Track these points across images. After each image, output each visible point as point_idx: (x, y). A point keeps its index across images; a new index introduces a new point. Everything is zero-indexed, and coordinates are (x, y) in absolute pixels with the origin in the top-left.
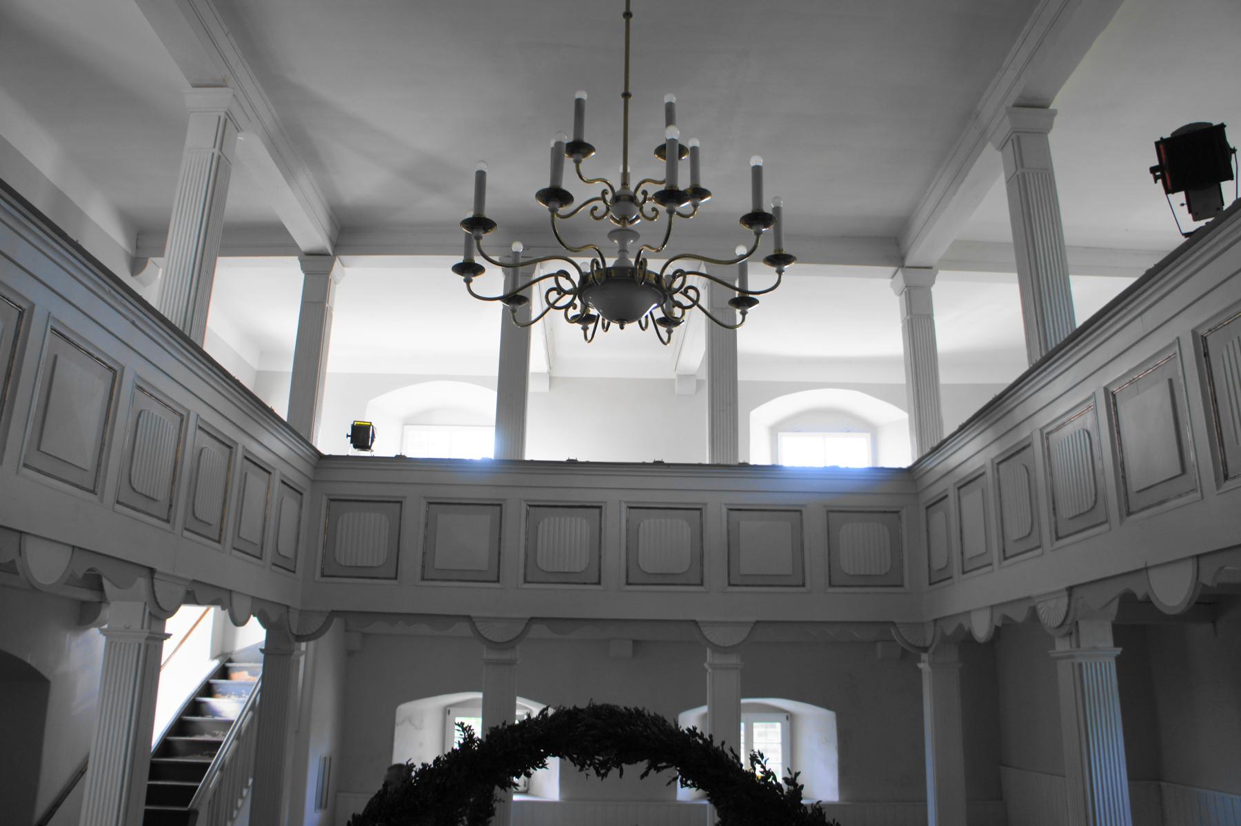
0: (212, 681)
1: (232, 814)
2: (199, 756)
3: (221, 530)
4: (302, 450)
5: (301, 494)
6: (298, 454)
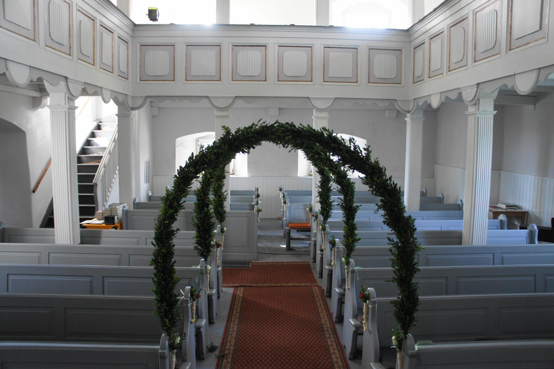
0: (94, 131)
1: (111, 185)
2: (93, 162)
3: (94, 59)
4: (127, 22)
5: (127, 43)
6: (124, 24)
